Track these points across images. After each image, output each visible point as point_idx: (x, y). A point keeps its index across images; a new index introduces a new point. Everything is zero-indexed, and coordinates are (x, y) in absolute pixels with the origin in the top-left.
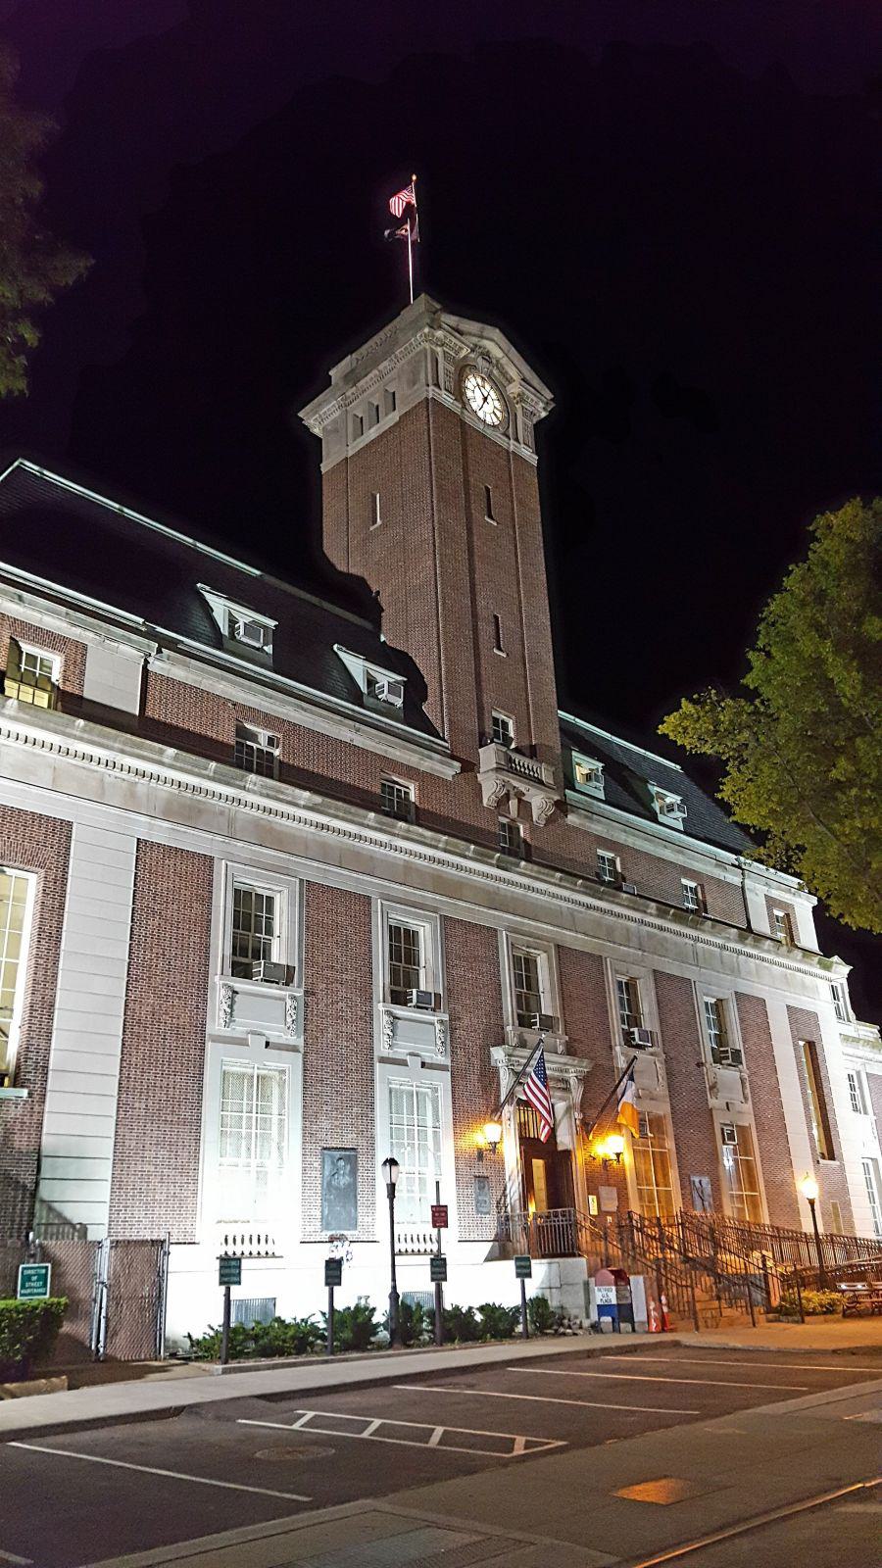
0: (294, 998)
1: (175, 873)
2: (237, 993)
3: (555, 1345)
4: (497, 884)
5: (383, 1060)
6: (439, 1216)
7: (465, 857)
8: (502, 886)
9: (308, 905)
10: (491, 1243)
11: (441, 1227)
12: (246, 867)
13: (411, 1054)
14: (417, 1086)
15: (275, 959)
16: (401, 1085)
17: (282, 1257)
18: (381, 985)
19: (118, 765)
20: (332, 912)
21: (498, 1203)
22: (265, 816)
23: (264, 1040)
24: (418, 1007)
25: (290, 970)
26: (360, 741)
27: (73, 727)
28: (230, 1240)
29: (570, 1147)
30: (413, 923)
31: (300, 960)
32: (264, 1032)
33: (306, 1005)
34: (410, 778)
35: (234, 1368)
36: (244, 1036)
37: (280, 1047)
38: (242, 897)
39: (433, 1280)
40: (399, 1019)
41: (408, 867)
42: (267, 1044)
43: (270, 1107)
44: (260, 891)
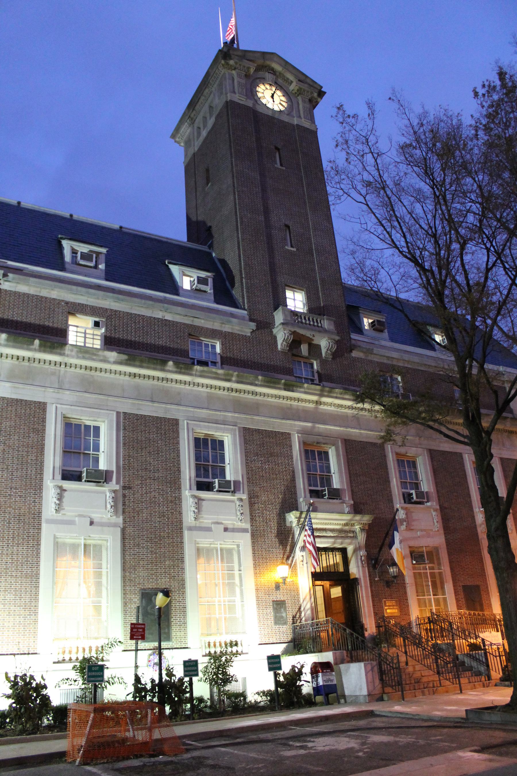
0: (241, 500)
1: (16, 416)
2: (65, 490)
3: (256, 720)
4: (289, 402)
5: (190, 529)
6: (137, 631)
7: (256, 385)
8: (295, 403)
9: (125, 429)
10: (286, 644)
11: (139, 639)
12: (73, 407)
13: (80, 516)
14: (220, 544)
15: (228, 478)
16: (211, 544)
17: (247, 653)
18: (188, 478)
19: (68, 364)
20: (261, 445)
21: (294, 617)
22: (88, 372)
23: (222, 527)
24: (88, 481)
25: (237, 483)
26: (159, 314)
27: (334, 393)
28: (212, 645)
29: (357, 576)
30: (218, 435)
31: (118, 467)
32: (223, 522)
33: (124, 496)
34: (213, 338)
35: (11, 740)
36: (210, 526)
37: (234, 530)
38: (201, 444)
39: (270, 669)
40: (203, 500)
41: (210, 398)
42: (92, 523)
43: (233, 566)
44: (88, 423)
